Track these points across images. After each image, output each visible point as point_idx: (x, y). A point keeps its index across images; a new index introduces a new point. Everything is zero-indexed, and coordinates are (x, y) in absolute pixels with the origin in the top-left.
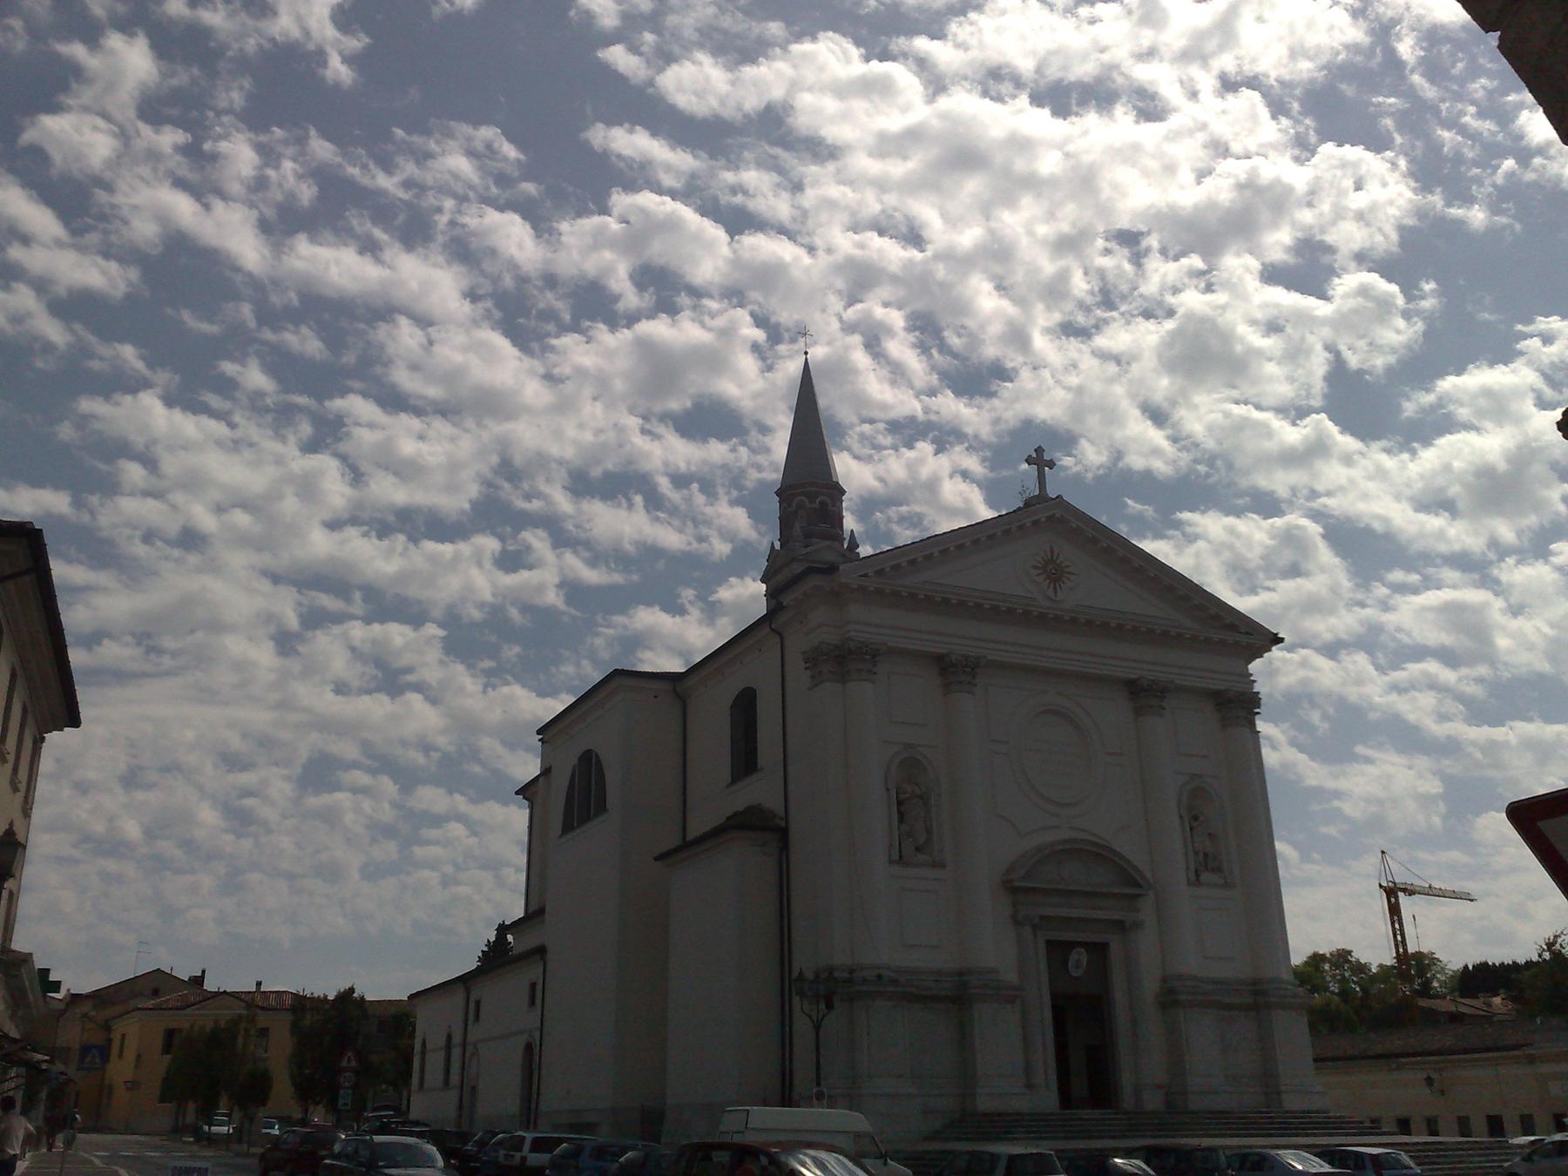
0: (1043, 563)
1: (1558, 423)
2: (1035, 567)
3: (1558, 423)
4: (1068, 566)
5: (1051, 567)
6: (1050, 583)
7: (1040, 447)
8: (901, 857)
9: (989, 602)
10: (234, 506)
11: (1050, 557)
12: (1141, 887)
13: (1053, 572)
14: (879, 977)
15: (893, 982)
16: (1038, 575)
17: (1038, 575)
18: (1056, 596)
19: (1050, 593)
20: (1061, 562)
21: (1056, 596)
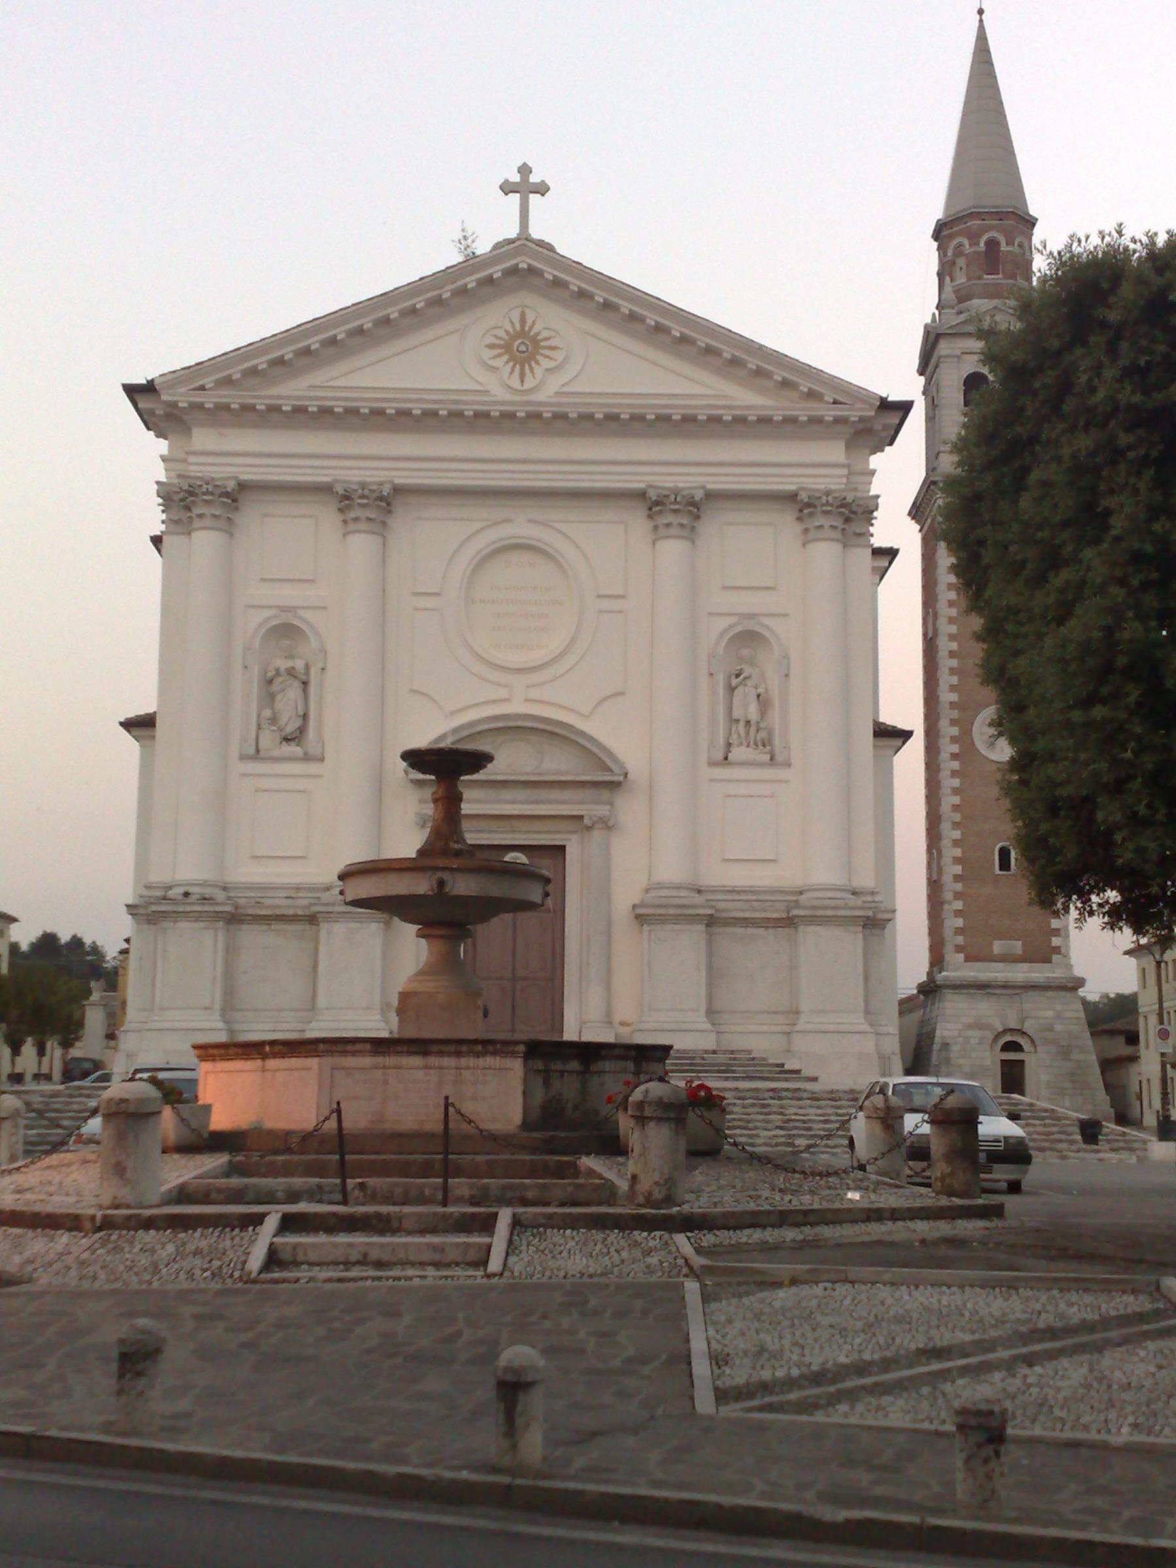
0: (506, 337)
1: (507, 181)
2: (491, 346)
3: (507, 181)
4: (546, 339)
5: (519, 341)
6: (514, 367)
7: (501, 188)
8: (258, 751)
9: (315, 403)
10: (430, 1264)
11: (518, 328)
12: (611, 771)
13: (523, 348)
14: (186, 894)
15: (204, 899)
16: (494, 357)
17: (494, 357)
18: (509, 378)
19: (515, 382)
20: (538, 334)
21: (509, 378)
